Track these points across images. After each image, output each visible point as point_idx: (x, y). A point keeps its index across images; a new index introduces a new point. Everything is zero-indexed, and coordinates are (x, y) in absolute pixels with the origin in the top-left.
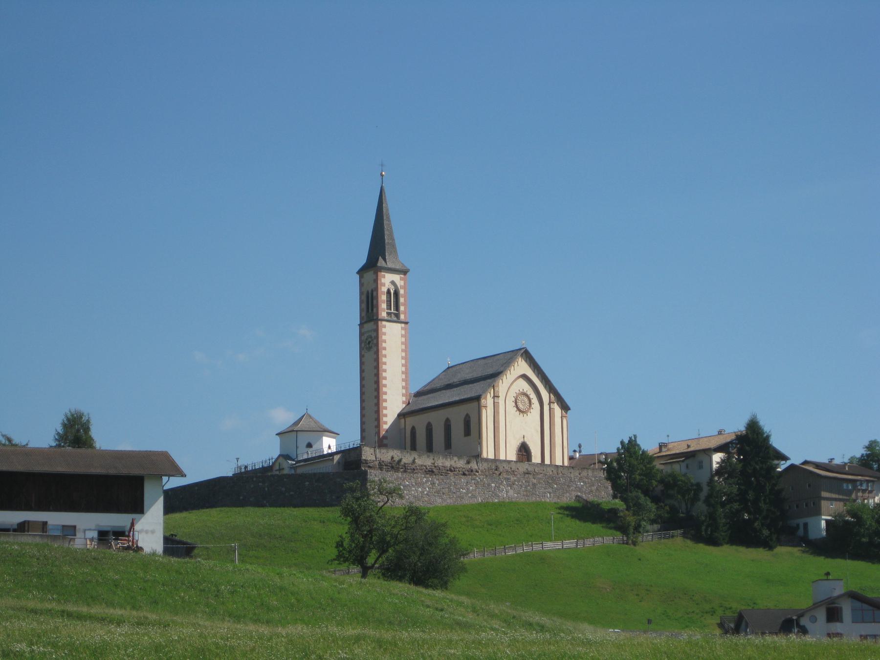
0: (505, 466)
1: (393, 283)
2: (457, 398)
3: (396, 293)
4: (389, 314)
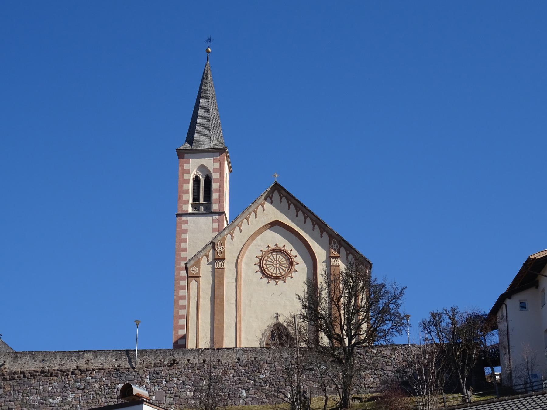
0: (191, 358)
1: (202, 168)
2: (505, 311)
3: (208, 181)
4: (194, 206)
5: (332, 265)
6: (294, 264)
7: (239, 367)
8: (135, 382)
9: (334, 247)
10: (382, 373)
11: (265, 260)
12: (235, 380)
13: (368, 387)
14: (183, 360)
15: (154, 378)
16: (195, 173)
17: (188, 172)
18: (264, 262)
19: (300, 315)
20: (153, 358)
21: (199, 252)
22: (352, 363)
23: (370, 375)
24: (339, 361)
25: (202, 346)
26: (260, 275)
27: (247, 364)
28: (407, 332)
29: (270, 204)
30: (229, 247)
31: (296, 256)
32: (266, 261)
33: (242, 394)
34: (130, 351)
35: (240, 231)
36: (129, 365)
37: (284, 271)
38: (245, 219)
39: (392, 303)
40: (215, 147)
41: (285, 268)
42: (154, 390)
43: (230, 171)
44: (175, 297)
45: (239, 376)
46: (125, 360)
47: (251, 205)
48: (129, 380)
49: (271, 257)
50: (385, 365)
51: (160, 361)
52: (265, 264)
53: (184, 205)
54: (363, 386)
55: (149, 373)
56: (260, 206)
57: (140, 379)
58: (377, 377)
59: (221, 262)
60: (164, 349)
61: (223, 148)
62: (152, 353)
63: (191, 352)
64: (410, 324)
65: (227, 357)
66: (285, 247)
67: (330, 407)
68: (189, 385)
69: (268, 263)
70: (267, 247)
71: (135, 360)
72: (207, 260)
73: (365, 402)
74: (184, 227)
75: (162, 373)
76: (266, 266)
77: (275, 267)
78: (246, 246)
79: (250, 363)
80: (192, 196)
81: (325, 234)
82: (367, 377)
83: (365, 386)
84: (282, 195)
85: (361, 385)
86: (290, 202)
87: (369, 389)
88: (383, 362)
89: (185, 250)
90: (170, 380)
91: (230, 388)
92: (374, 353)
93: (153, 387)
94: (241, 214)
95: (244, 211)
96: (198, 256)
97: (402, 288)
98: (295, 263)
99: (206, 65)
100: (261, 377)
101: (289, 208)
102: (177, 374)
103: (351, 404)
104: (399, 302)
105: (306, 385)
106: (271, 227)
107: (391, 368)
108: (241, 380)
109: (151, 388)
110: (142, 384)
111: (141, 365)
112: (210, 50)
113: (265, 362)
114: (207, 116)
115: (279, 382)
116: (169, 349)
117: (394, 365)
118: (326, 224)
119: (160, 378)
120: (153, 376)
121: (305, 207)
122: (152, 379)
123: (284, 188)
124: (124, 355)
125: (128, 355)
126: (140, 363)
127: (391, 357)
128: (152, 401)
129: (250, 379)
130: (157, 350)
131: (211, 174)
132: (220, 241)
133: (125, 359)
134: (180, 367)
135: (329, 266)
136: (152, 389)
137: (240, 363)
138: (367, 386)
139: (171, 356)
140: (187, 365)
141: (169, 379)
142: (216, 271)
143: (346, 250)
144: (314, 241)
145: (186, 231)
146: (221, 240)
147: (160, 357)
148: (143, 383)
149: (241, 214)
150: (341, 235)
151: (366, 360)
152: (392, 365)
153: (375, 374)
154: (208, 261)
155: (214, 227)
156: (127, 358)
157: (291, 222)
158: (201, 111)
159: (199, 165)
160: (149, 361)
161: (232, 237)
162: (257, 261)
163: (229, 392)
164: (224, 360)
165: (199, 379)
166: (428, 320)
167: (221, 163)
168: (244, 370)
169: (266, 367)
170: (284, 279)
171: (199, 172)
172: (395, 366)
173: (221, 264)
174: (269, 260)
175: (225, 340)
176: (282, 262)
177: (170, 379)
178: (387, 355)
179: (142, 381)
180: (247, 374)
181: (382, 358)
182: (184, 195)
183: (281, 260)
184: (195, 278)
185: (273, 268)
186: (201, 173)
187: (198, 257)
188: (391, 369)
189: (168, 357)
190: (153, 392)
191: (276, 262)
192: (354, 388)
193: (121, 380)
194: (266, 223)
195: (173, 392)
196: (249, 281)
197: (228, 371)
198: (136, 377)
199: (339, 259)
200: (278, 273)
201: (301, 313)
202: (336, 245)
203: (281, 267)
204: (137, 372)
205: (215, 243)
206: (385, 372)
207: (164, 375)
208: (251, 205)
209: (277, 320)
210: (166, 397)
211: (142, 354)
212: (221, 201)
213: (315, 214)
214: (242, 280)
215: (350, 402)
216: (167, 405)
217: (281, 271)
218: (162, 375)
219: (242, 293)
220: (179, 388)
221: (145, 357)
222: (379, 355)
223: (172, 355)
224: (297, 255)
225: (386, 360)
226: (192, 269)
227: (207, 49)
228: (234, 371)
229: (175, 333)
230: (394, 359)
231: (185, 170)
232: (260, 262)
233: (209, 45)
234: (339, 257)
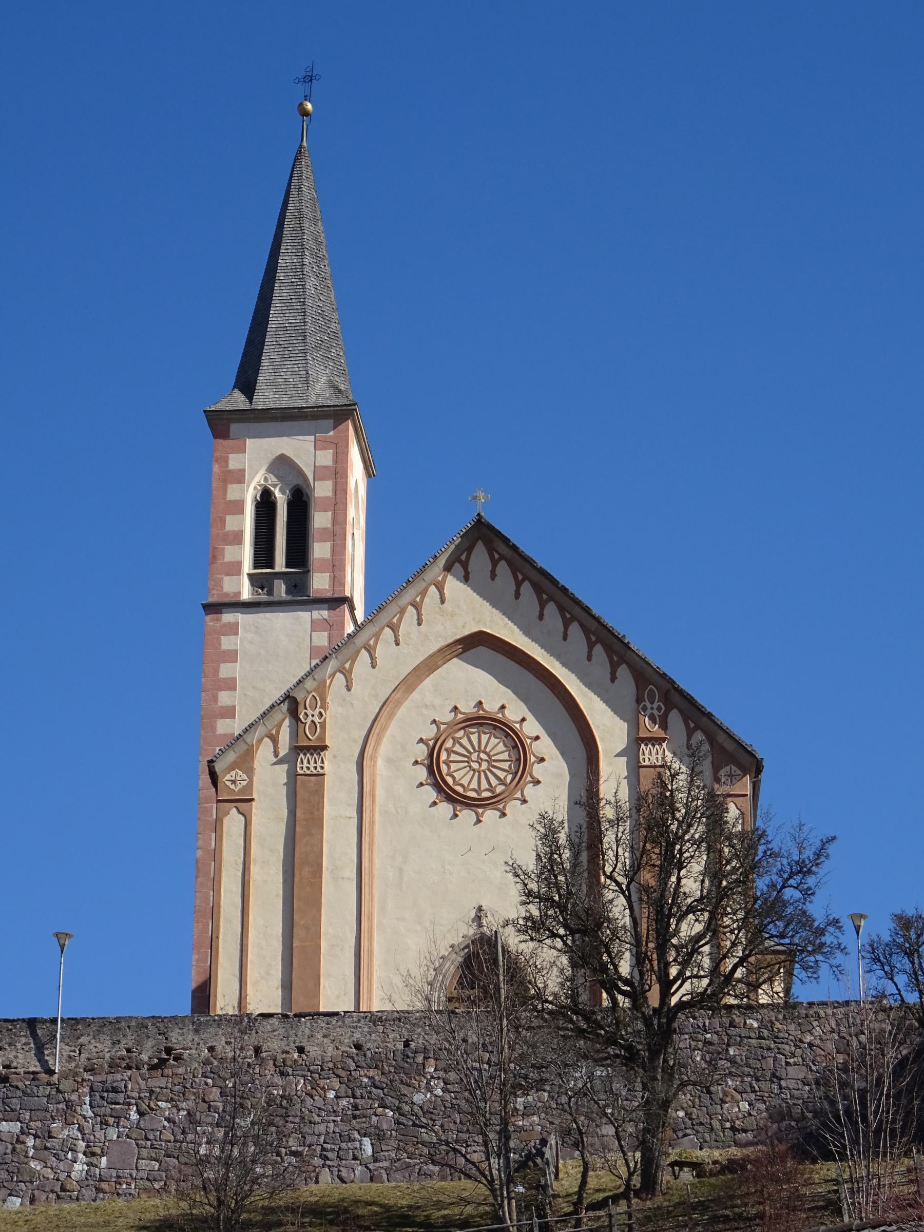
5: (643, 764)
6: (532, 761)
7: (355, 1070)
8: (49, 1116)
9: (649, 712)
10: (773, 1086)
11: (446, 750)
12: (343, 1109)
13: (733, 1129)
14: (196, 1049)
15: (106, 1104)
16: (262, 482)
17: (239, 477)
18: (444, 756)
19: (524, 918)
20: (108, 1043)
21: (251, 725)
22: (671, 1063)
23: (739, 1093)
24: (631, 1058)
25: (255, 1006)
26: (430, 794)
27: (376, 1062)
28: (835, 969)
29: (461, 582)
30: (340, 710)
31: (537, 738)
32: (449, 752)
33: (361, 1149)
34: (39, 1022)
35: (372, 663)
36: (37, 1064)
37: (502, 782)
38: (388, 626)
39: (792, 886)
40: (321, 402)
41: (506, 773)
42: (105, 1137)
43: (369, 473)
44: (199, 853)
45: (354, 1097)
46: (26, 1048)
47: (404, 585)
48: (31, 1110)
49: (465, 741)
50: (784, 1064)
51: (129, 1051)
52: (444, 762)
53: (228, 577)
54: (716, 1124)
55: (92, 1089)
56: (433, 588)
57: (62, 1106)
58: (758, 1097)
59: (315, 755)
60: (140, 1015)
61: (346, 405)
62: (105, 1029)
63: (219, 1026)
64: (845, 948)
65: (325, 1040)
66: (506, 711)
67: (611, 1191)
69: (453, 757)
70: (451, 712)
71: (56, 1048)
72: (272, 750)
73: (712, 1174)
74: (226, 643)
75: (130, 1087)
76: (449, 767)
77: (474, 770)
78: (388, 709)
80: (252, 552)
81: (623, 672)
82: (728, 1099)
83: (721, 1125)
84: (497, 556)
85: (711, 1124)
86: (520, 577)
87: (735, 1135)
88: (777, 1055)
89: (229, 712)
90: (152, 1109)
91: (328, 1133)
92: (751, 1028)
93: (101, 1129)
94: (375, 612)
95: (384, 604)
96: (247, 737)
97: (822, 841)
98: (533, 759)
99: (299, 152)
100: (418, 1098)
101: (517, 595)
102: (172, 1091)
103: (664, 1182)
104: (811, 881)
106: (465, 650)
107: (801, 1073)
108: (360, 1108)
109: (95, 1133)
110: (70, 1119)
111: (73, 1065)
112: (309, 106)
113: (431, 1055)
114: (299, 307)
116: (153, 1017)
117: (811, 1064)
118: (626, 641)
119: (123, 1104)
120: (102, 1098)
121: (564, 590)
122: (98, 1107)
123: (503, 536)
124: (22, 1033)
125: (34, 1034)
126: (70, 1057)
127: (801, 1041)
128: (97, 1170)
129: (385, 1107)
130: (118, 1020)
131: (308, 485)
132: (313, 693)
133: (24, 1044)
134: (181, 1070)
135: (635, 767)
136: (100, 1134)
137: (356, 1058)
138: (728, 1125)
139: (160, 1037)
140: (206, 1062)
141: (149, 1106)
142: (299, 782)
143: (686, 718)
144: (590, 691)
145: (231, 657)
146: (315, 690)
147: (129, 1040)
148: (74, 1117)
149: (375, 612)
150: (670, 674)
151: (727, 1050)
152: (803, 1065)
153: (754, 1091)
154: (276, 754)
155: (316, 642)
156: (32, 1041)
157: (523, 636)
158: (280, 293)
159: (274, 457)
160: (94, 1050)
161: (347, 681)
162: (422, 752)
163: (325, 1142)
164: (316, 1048)
166: (886, 938)
167: (339, 451)
168: (369, 1077)
169: (432, 1070)
170: (501, 806)
171: (272, 479)
172: (814, 1068)
173: (315, 762)
174: (457, 748)
175: (324, 987)
176: (494, 755)
177: (152, 1105)
178: (789, 1035)
179: (69, 1111)
180: (378, 1090)
181: (775, 1042)
182: (227, 547)
183: (493, 749)
184: (238, 804)
185: (486, 747)
186: (279, 480)
187: (248, 741)
188: (801, 1076)
189: (151, 1039)
190: (101, 1144)
191: (478, 755)
192: (688, 1131)
193: (8, 1108)
194: (450, 640)
195: (162, 1145)
196: (397, 813)
197: (322, 1083)
198: (54, 1101)
199: (664, 745)
201: (528, 915)
202: (655, 705)
203: (494, 770)
204: (56, 1084)
205: (299, 700)
206: (783, 1083)
207: (135, 1095)
208: (404, 585)
209: (480, 926)
210: (138, 1158)
211: (75, 1030)
212: (336, 566)
213: (596, 611)
214: (377, 810)
215: (662, 1175)
217: (494, 782)
218: (129, 1093)
221: (83, 1040)
222: (766, 1033)
223: (164, 1034)
224: (540, 735)
225: (787, 1047)
226: (228, 777)
227: (301, 104)
228: (340, 1082)
229: (198, 961)
230: (811, 1045)
231: (231, 471)
232: (431, 755)
233: (307, 93)
234: (664, 740)
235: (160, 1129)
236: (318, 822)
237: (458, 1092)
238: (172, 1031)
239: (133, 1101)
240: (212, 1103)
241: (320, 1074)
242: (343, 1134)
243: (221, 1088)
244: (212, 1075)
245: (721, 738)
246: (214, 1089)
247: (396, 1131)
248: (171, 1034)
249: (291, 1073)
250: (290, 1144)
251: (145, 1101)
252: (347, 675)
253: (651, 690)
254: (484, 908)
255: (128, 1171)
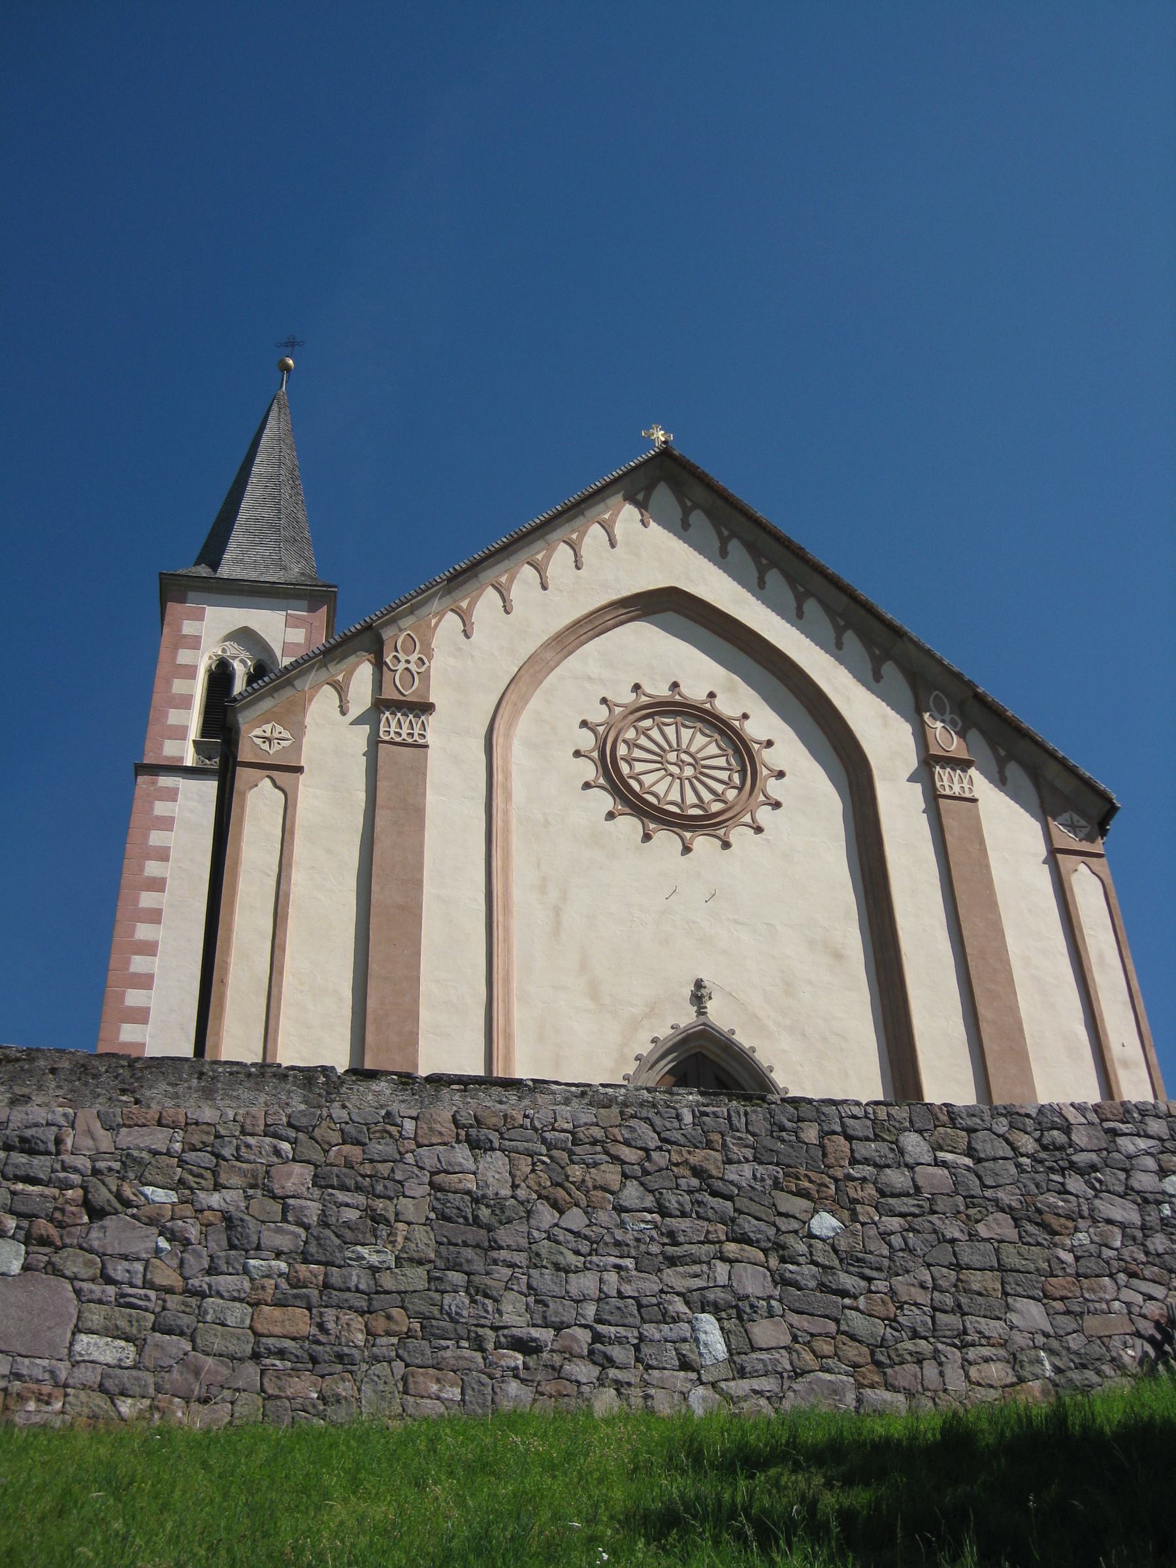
1: (245, 636)
7: (660, 1149)
12: (638, 1240)
17: (194, 643)
33: (697, 1340)
45: (664, 1212)
68: (278, 1255)
74: (161, 808)
75: (69, 1142)
79: (732, 1128)
90: (127, 1204)
105: (1140, 1298)
115: (958, 1267)
130: (31, 1055)
165: (358, 1213)
170: (721, 832)
177: (128, 1191)
184: (275, 774)
185: (689, 745)
195: (147, 1298)
200: (688, 802)
207: (83, 1163)
209: (701, 1012)
210: (77, 1330)
216: (83, 1395)
219: (515, 875)
220: (196, 1263)
231: (185, 636)
235: (144, 1256)
236: (416, 814)
237: (914, 1215)
238: (150, 1087)
239: (75, 1178)
240: (291, 1201)
241: (571, 1153)
242: (645, 1301)
243: (316, 1166)
244: (292, 1134)
245: (1051, 771)
246: (297, 1168)
247: (780, 1301)
248: (148, 1093)
249: (496, 1144)
250: (507, 1319)
251: (108, 1180)
252: (465, 617)
253: (937, 696)
254: (706, 983)
255: (45, 1362)
